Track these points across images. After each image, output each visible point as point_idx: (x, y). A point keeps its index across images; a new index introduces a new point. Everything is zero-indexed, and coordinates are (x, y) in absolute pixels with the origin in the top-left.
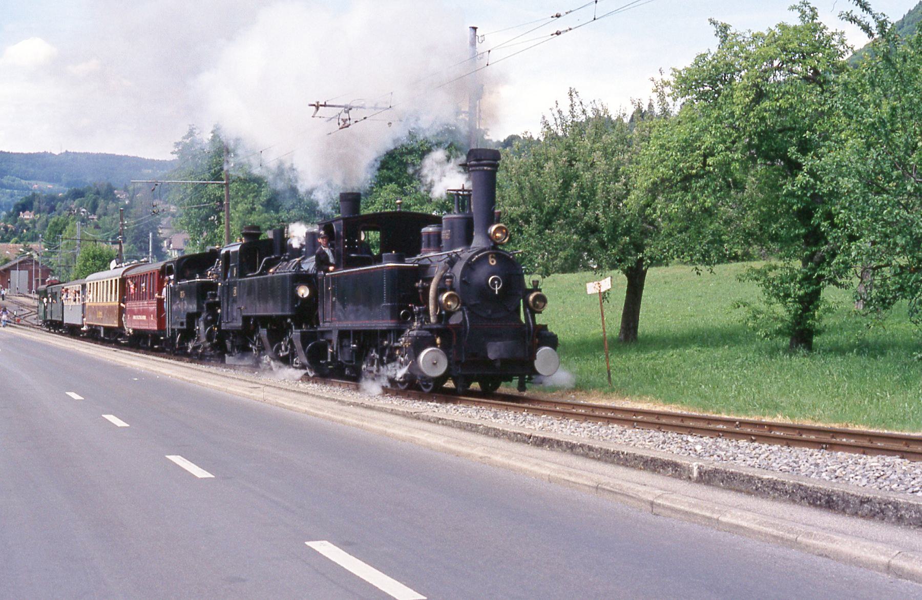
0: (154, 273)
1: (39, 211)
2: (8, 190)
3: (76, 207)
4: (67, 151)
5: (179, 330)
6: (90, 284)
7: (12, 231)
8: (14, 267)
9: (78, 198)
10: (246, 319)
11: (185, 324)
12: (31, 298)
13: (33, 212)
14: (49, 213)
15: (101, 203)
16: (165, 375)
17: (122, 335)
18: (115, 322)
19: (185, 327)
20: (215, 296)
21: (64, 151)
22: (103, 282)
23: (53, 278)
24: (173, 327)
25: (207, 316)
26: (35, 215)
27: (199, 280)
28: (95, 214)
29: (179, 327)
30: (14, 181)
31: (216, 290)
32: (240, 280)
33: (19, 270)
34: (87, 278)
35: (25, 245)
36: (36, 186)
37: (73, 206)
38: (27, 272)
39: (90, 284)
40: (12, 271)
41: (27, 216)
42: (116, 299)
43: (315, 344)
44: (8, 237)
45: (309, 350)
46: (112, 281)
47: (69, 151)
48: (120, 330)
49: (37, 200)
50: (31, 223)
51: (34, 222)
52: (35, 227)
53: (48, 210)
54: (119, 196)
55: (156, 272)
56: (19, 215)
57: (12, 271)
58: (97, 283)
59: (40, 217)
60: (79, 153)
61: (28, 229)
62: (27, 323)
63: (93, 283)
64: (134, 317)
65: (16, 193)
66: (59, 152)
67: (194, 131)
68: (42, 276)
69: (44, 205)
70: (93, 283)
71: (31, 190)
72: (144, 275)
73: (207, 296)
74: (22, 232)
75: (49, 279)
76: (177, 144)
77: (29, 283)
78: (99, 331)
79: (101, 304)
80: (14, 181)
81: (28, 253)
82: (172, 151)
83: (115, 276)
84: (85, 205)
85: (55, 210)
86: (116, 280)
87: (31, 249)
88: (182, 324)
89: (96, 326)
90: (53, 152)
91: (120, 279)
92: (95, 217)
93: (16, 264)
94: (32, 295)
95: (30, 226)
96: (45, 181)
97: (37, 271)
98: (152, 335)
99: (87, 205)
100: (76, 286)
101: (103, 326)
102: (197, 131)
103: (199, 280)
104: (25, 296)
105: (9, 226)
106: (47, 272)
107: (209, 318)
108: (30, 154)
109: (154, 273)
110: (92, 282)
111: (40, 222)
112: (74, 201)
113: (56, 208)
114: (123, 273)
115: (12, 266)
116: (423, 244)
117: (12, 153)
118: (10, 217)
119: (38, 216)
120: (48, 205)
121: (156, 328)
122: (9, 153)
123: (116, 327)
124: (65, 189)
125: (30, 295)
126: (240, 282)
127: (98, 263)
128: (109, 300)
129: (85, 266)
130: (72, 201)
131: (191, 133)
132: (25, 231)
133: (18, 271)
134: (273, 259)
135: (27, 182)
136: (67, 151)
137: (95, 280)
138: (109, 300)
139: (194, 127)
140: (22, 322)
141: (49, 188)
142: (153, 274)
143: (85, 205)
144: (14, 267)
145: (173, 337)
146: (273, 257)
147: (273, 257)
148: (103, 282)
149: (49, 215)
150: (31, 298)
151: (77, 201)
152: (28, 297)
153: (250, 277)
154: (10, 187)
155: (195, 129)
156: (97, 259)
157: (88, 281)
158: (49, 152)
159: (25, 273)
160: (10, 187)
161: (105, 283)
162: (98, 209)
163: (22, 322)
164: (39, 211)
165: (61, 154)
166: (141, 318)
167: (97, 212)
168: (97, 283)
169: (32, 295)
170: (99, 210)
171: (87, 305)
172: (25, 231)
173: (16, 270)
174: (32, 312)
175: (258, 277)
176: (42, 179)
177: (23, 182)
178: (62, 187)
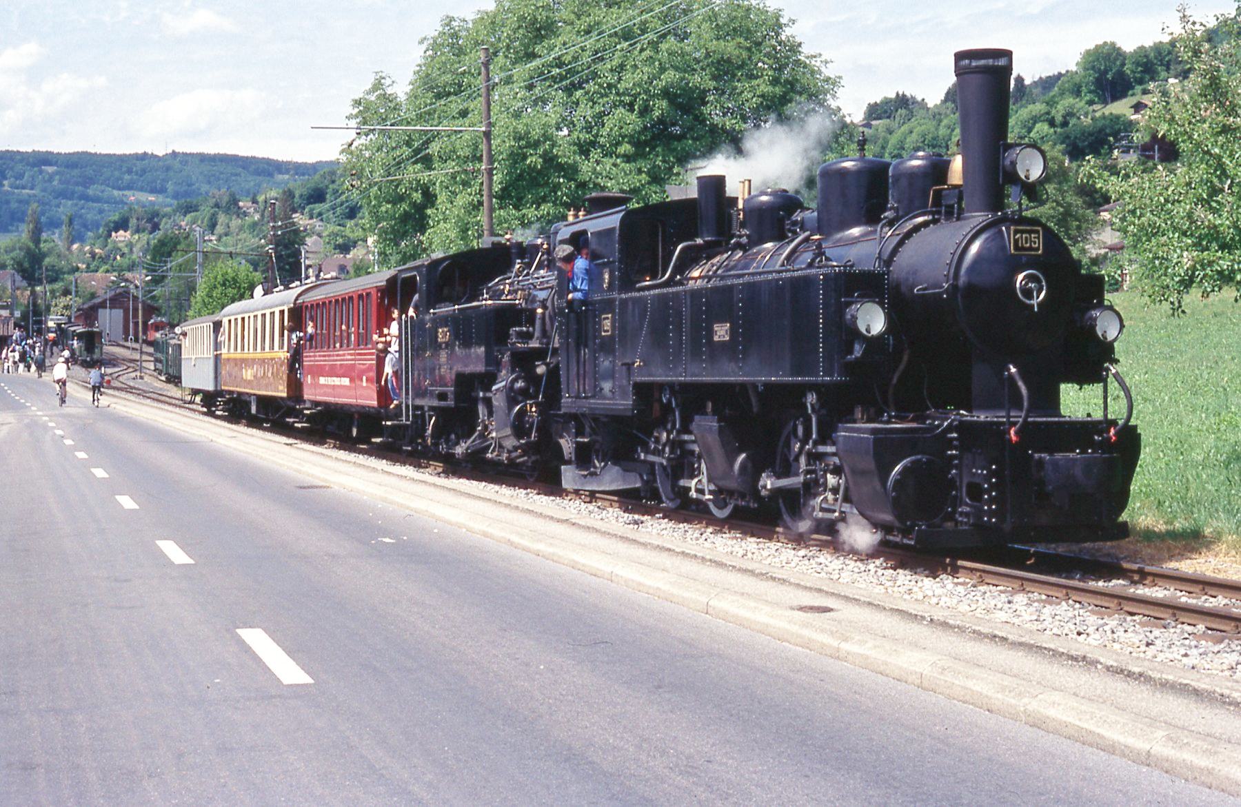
0: (368, 294)
1: (138, 230)
2: (95, 205)
3: (187, 225)
4: (173, 151)
5: (432, 408)
6: (230, 321)
7: (100, 257)
8: (102, 305)
9: (191, 212)
10: (644, 392)
11: (451, 396)
12: (128, 348)
13: (129, 232)
14: (151, 233)
15: (222, 218)
16: (450, 523)
17: (298, 414)
18: (281, 388)
19: (451, 403)
20: (528, 336)
21: (170, 151)
22: (256, 316)
23: (159, 319)
24: (419, 402)
25: (515, 380)
26: (132, 236)
27: (490, 302)
28: (213, 234)
29: (435, 403)
30: (103, 191)
31: (533, 324)
32: (623, 296)
33: (110, 308)
34: (227, 310)
35: (119, 275)
36: (133, 198)
37: (183, 224)
38: (122, 311)
39: (230, 321)
40: (100, 311)
41: (121, 236)
42: (281, 347)
43: (913, 462)
44: (96, 266)
45: (897, 482)
46: (273, 314)
47: (177, 151)
48: (291, 404)
49: (135, 216)
50: (126, 246)
51: (130, 245)
52: (131, 251)
53: (149, 229)
54: (245, 209)
55: (373, 292)
56: (111, 236)
57: (100, 311)
58: (243, 319)
59: (139, 238)
60: (190, 154)
61: (122, 255)
62: (123, 386)
63: (236, 319)
64: (322, 380)
65: (106, 208)
66: (164, 153)
67: (383, 81)
68: (144, 316)
69: (143, 222)
70: (236, 319)
71: (126, 204)
72: (343, 299)
73: (508, 336)
74: (115, 259)
75: (152, 321)
76: (357, 103)
77: (124, 326)
78: (248, 404)
79: (232, 356)
80: (103, 191)
81: (123, 284)
82: (348, 114)
83: (242, 313)
84: (199, 222)
85: (159, 230)
86: (282, 312)
87: (126, 280)
88: (442, 397)
89: (240, 394)
90: (155, 153)
91: (289, 310)
92: (213, 238)
93: (106, 300)
94: (129, 344)
95: (126, 250)
96: (146, 191)
97: (136, 310)
98: (360, 414)
99: (202, 223)
100: (206, 325)
101: (254, 395)
102: (387, 82)
103: (490, 302)
104: (118, 345)
105: (97, 251)
106: (150, 310)
107: (520, 384)
108: (125, 155)
109: (368, 294)
110: (232, 318)
111: (139, 246)
112: (185, 216)
113: (161, 227)
114: (297, 299)
115: (100, 303)
116: (905, 231)
117: (100, 154)
118: (98, 238)
119: (136, 237)
120: (150, 223)
121: (375, 403)
122: (96, 154)
123: (282, 398)
124: (172, 202)
125: (126, 344)
126: (624, 303)
127: (231, 292)
128: (267, 349)
129: (211, 297)
130: (182, 217)
131: (378, 85)
132: (118, 257)
133: (108, 310)
134: (699, 246)
135: (121, 193)
136: (173, 151)
137: (239, 313)
138: (267, 349)
139: (384, 75)
140: (115, 384)
141: (151, 201)
142: (363, 297)
143: (199, 222)
144: (102, 305)
145: (420, 421)
146: (699, 241)
147: (699, 241)
148: (256, 316)
149: (151, 236)
150: (128, 348)
151: (189, 217)
152: (124, 346)
153: (649, 288)
154: (97, 200)
155: (384, 78)
156: (230, 286)
157: (224, 316)
158: (150, 153)
159: (118, 313)
160: (97, 200)
161: (259, 318)
162: (218, 227)
163: (115, 384)
164: (138, 231)
165: (167, 154)
166: (338, 383)
167: (215, 232)
168: (243, 319)
169: (129, 344)
170: (219, 229)
171: (223, 356)
172: (118, 257)
173: (106, 308)
174: (129, 367)
175: (665, 290)
176: (142, 189)
177: (116, 193)
178: (169, 200)
